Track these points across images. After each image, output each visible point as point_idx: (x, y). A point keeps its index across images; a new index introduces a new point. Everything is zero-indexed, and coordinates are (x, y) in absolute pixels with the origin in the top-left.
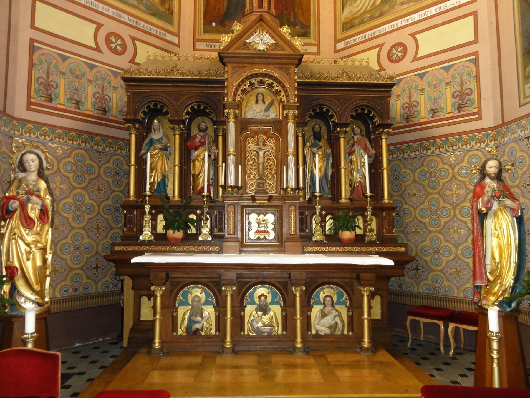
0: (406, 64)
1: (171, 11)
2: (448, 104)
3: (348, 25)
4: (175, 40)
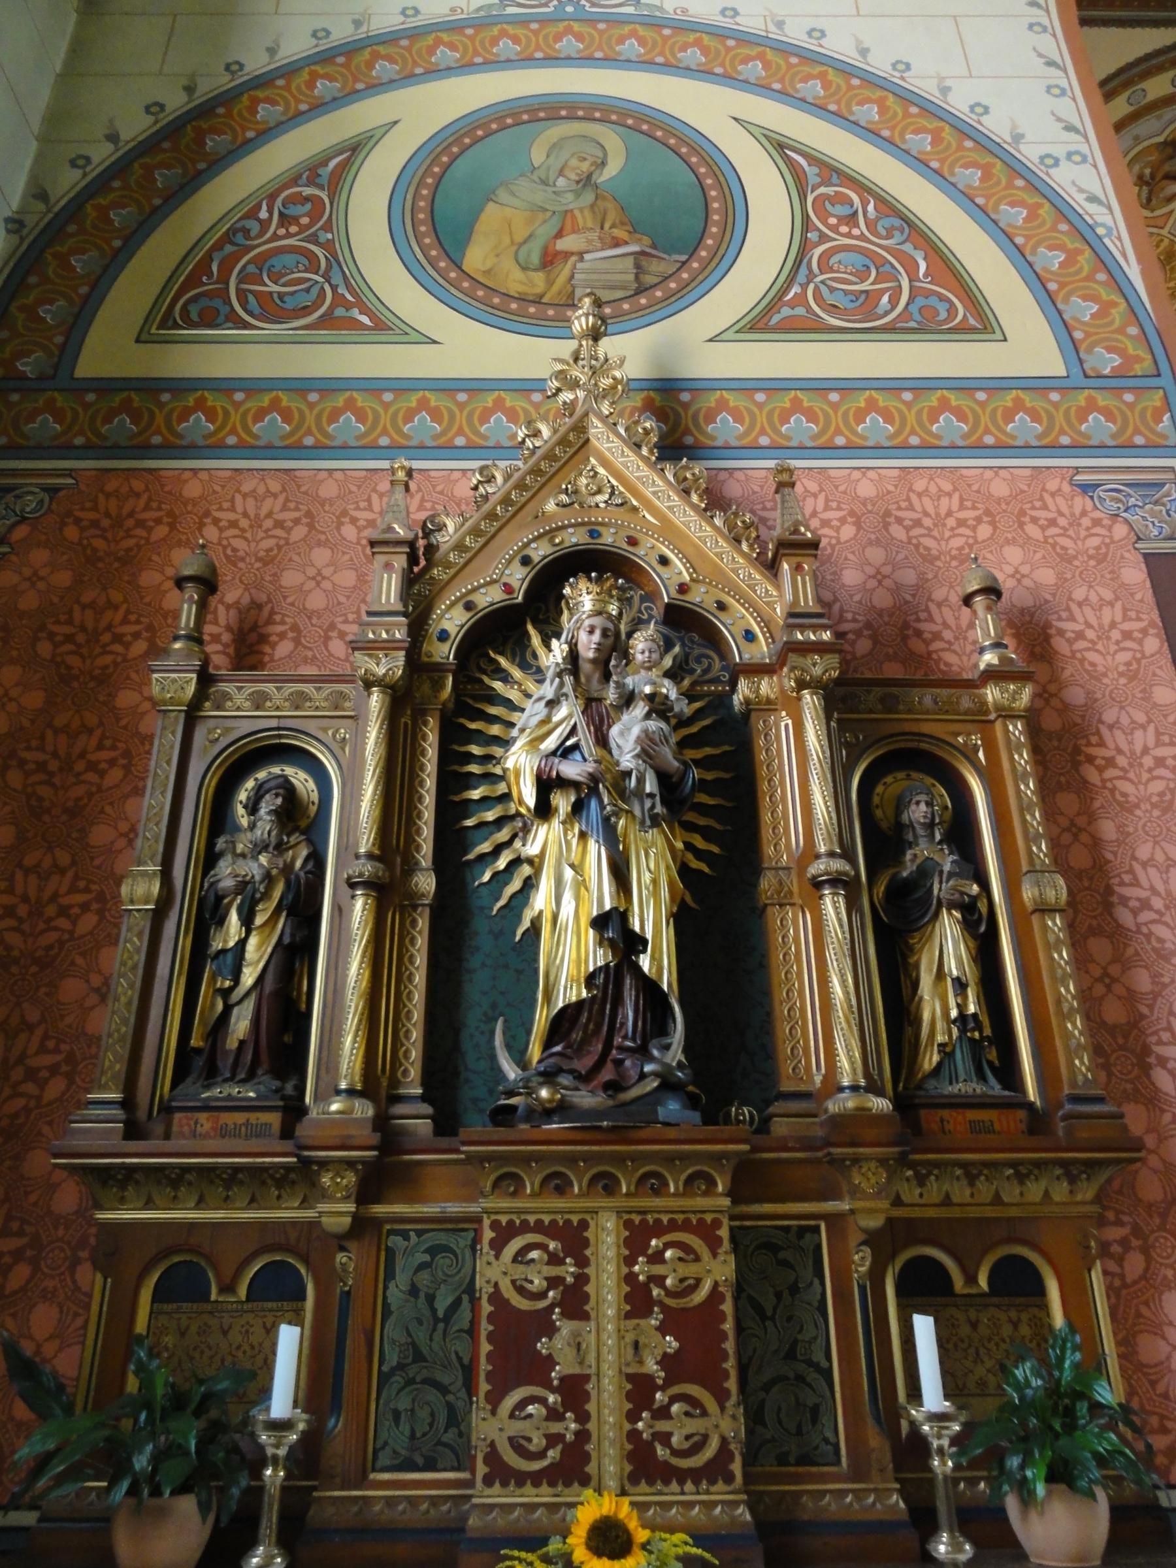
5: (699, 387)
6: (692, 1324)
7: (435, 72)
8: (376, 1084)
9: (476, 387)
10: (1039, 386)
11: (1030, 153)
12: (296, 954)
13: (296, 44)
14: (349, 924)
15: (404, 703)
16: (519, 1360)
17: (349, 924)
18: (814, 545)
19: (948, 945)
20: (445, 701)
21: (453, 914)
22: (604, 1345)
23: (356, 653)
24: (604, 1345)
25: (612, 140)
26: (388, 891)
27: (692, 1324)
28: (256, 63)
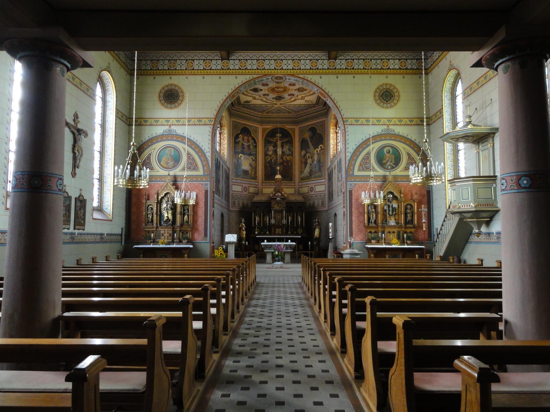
0: (313, 193)
1: (256, 177)
2: (320, 204)
3: (302, 179)
4: (257, 184)
5: (178, 176)
6: (170, 234)
7: (159, 142)
8: (157, 224)
9: (162, 176)
10: (201, 176)
11: (205, 151)
12: (153, 217)
13: (147, 138)
14: (155, 216)
15: (157, 203)
16: (163, 235)
17: (155, 216)
18: (78, 260)
19: (186, 217)
20: (159, 203)
21: (161, 215)
22: (166, 235)
23: (167, 174)
24: (166, 235)
25: (172, 149)
26: (157, 214)
27: (170, 234)
28: (144, 141)
